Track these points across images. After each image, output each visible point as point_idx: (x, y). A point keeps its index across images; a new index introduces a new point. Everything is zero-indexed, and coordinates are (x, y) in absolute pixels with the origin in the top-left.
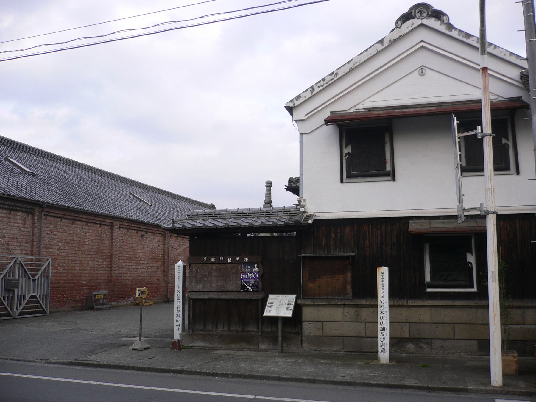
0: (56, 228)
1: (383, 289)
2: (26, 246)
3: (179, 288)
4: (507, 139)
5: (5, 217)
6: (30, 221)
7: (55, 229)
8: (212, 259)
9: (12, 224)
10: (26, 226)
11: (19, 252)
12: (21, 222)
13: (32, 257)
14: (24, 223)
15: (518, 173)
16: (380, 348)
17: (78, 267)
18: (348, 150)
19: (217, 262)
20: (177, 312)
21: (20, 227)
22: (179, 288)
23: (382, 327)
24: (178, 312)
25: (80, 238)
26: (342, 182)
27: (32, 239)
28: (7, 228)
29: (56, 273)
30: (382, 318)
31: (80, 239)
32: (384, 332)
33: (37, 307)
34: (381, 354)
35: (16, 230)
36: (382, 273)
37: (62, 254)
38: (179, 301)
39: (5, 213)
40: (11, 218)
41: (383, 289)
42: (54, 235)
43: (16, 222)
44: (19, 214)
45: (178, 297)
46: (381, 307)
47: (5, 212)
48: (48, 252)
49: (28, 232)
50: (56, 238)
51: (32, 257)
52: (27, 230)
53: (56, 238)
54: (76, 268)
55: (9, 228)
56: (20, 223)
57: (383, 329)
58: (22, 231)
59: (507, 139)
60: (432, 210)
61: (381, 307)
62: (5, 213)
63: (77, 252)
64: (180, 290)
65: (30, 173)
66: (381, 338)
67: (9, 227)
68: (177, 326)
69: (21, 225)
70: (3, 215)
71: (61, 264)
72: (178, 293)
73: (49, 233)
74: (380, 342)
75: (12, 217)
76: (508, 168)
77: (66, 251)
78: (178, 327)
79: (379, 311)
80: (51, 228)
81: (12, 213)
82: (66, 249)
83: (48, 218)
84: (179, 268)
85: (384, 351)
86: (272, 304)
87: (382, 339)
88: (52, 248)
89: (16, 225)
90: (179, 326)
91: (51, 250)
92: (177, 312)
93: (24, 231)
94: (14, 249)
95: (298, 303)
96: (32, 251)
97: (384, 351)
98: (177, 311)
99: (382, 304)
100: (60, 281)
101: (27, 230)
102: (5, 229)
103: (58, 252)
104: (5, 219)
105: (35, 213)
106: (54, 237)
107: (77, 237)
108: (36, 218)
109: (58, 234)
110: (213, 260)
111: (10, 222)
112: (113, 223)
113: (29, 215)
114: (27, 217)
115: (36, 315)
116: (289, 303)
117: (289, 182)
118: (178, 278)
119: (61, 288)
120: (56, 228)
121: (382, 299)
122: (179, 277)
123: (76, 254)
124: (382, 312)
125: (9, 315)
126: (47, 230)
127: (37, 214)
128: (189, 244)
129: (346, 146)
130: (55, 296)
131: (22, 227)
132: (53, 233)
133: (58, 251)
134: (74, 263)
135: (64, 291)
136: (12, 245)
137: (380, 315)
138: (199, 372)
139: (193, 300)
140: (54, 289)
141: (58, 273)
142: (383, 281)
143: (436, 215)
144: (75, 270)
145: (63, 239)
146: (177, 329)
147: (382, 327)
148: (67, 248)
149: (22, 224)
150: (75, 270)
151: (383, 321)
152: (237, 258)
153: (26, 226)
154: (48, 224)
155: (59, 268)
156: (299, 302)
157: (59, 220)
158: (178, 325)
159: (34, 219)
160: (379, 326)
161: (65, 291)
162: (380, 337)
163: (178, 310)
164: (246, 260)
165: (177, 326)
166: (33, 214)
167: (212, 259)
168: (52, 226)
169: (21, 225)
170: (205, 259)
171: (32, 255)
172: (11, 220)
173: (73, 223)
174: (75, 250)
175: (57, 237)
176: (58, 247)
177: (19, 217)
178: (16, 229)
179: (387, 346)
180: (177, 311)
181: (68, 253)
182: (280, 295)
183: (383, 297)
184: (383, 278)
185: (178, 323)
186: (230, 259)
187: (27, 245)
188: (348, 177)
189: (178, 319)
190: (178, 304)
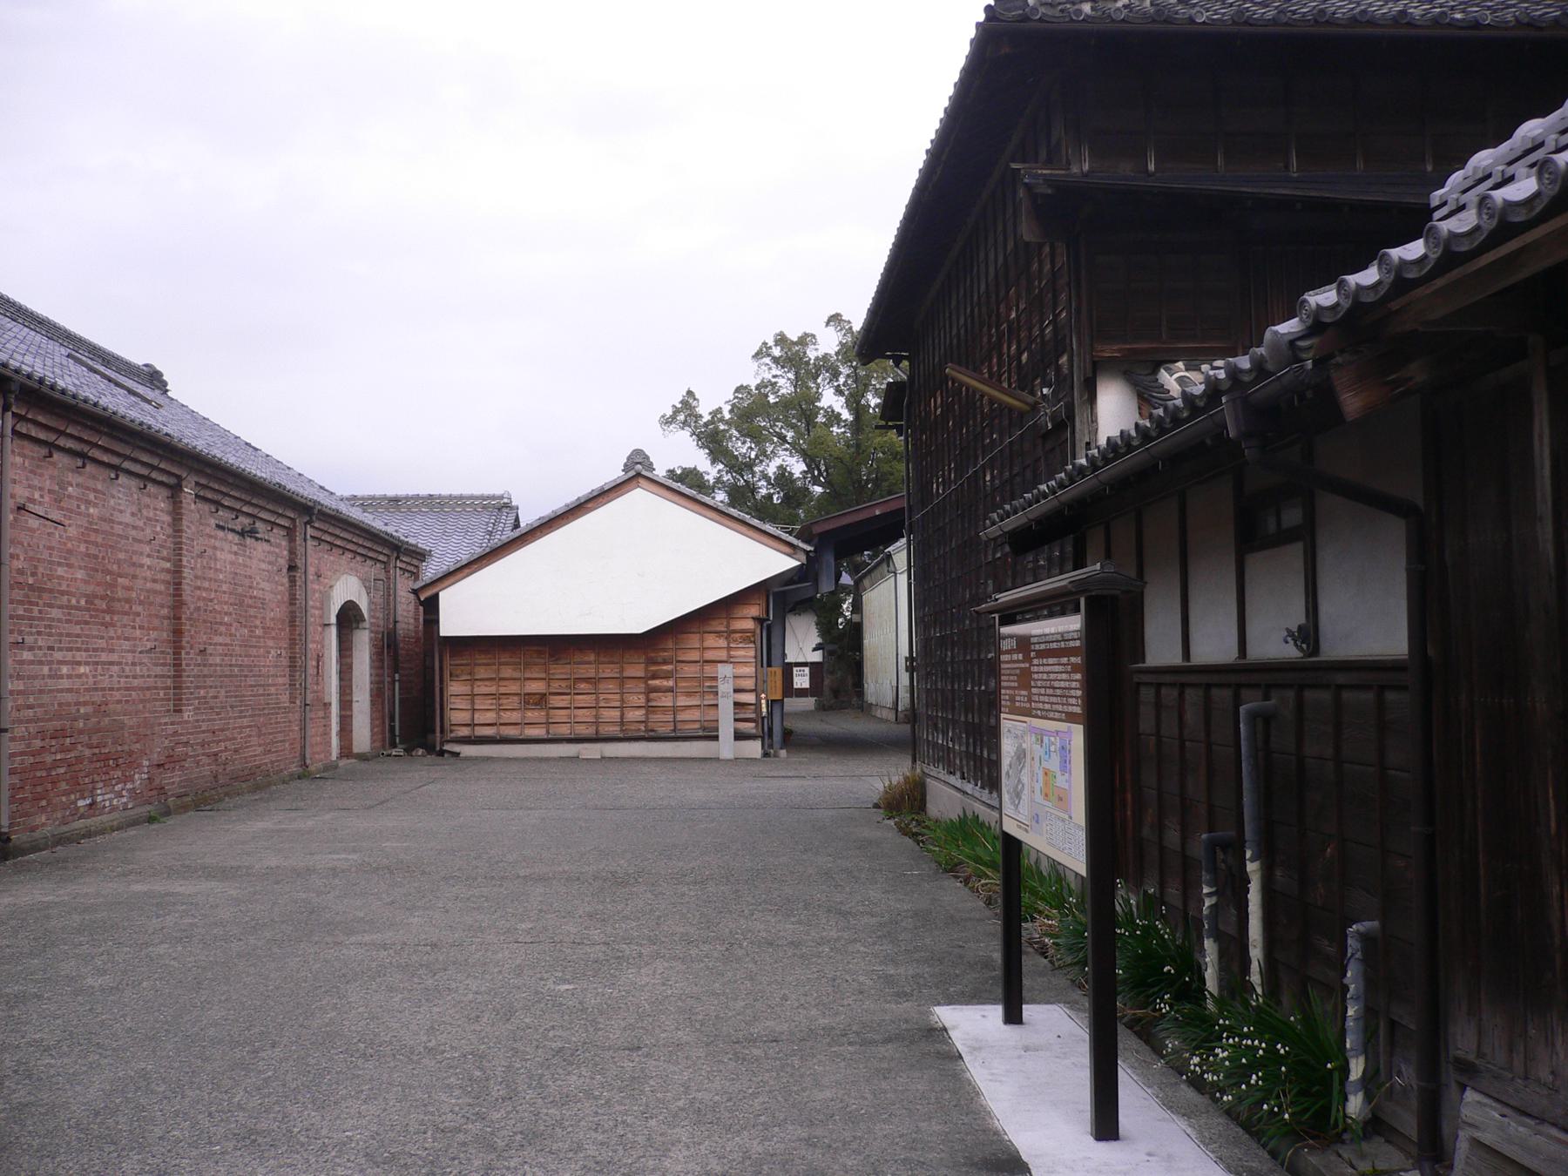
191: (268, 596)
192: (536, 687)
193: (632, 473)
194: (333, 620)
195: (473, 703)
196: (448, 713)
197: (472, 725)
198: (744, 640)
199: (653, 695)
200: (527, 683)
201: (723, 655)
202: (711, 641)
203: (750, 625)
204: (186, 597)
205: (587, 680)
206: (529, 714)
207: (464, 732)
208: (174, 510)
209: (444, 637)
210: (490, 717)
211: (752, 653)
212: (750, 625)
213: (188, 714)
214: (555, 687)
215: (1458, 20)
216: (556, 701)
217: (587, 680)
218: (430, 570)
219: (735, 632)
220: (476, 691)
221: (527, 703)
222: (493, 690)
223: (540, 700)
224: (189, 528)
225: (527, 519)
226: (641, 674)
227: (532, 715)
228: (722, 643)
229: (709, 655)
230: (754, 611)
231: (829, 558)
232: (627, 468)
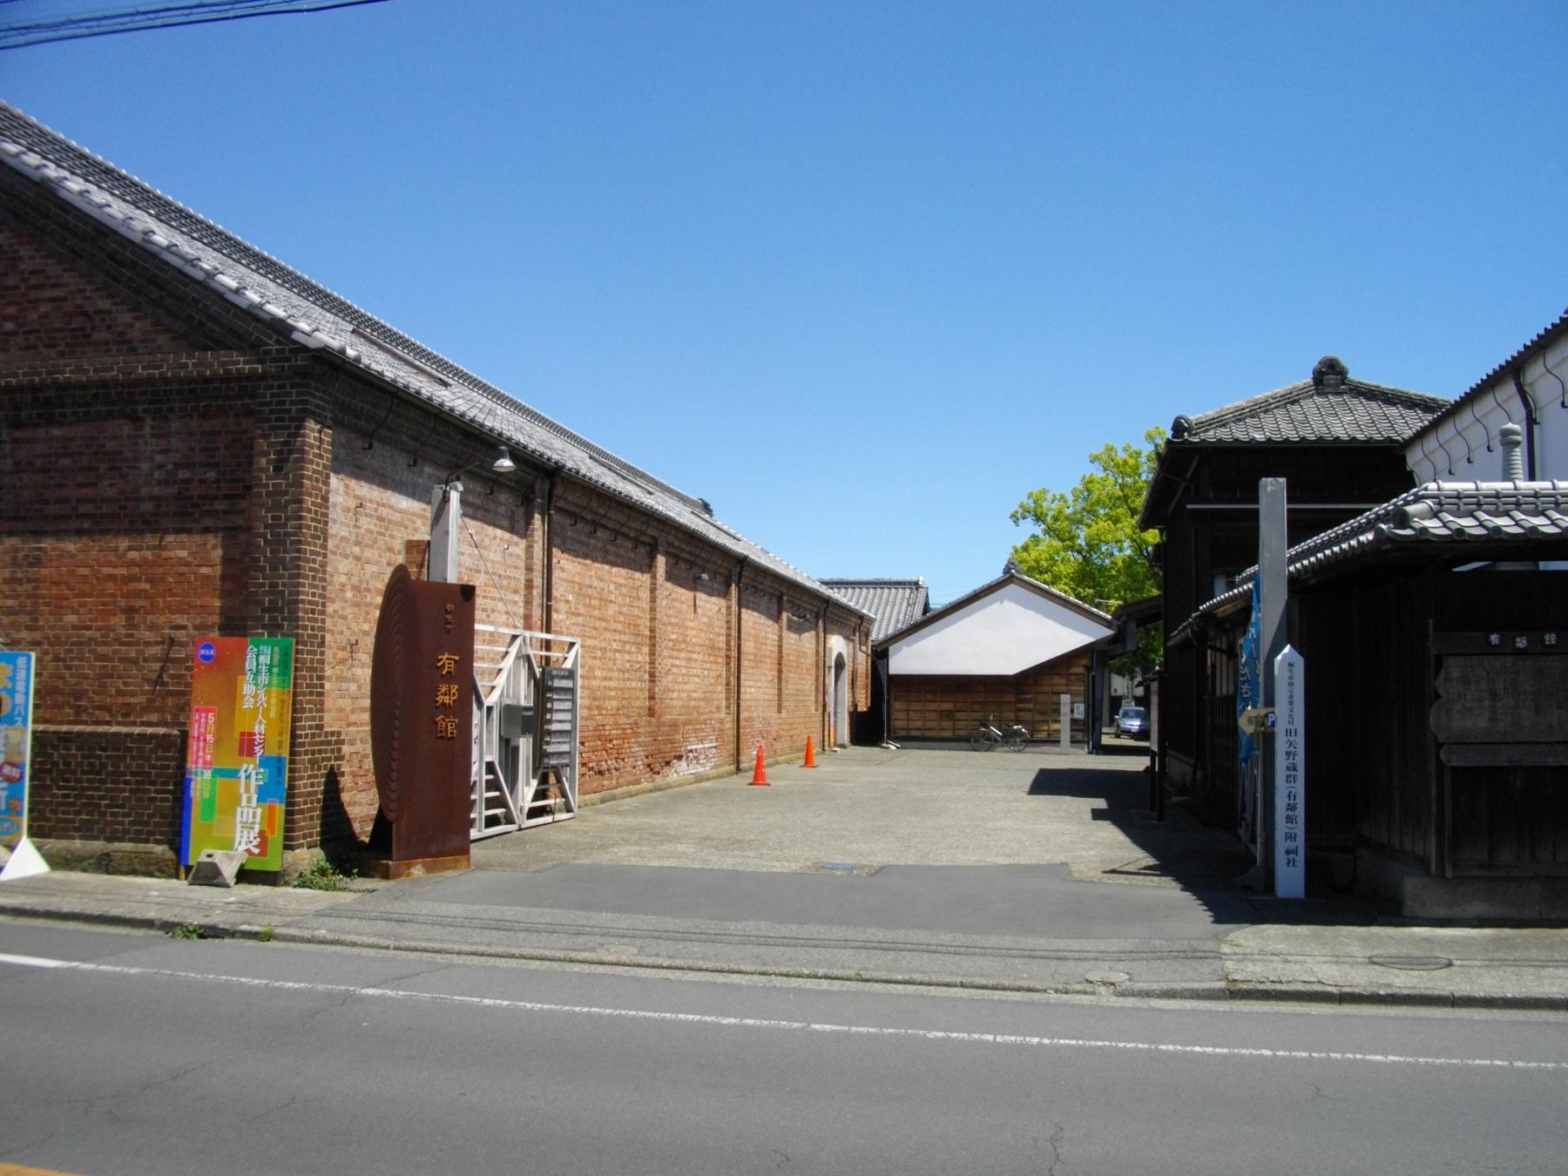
3: (1293, 734)
8: (1518, 640)
20: (1288, 809)
22: (1293, 734)
24: (1291, 807)
27: (526, 580)
31: (601, 585)
45: (1291, 761)
57: (1290, 837)
64: (1295, 739)
68: (1288, 852)
72: (1292, 749)
77: (580, 620)
78: (1291, 856)
84: (1291, 671)
90: (1296, 852)
92: (1288, 809)
98: (1289, 805)
110: (1521, 643)
112: (655, 539)
117: (1173, 429)
118: (1288, 700)
122: (1291, 697)
128: (377, 613)
139: (1456, 771)
146: (1288, 863)
148: (582, 610)
158: (1291, 848)
163: (1292, 801)
165: (1288, 852)
167: (1518, 640)
173: (591, 533)
180: (1289, 805)
185: (1291, 845)
189: (1293, 831)
190: (1292, 785)
191: (808, 651)
192: (948, 706)
193: (1008, 576)
194: (833, 664)
195: (908, 715)
196: (892, 722)
197: (908, 729)
198: (1077, 680)
199: (1019, 714)
200: (927, 704)
201: (1064, 688)
202: (1057, 680)
203: (1081, 670)
204: (784, 654)
205: (979, 703)
206: (942, 723)
207: (903, 733)
208: (213, 532)
209: (236, 679)
210: (918, 724)
211: (1082, 688)
212: (1081, 670)
213: (784, 714)
214: (959, 706)
215: (1046, 1045)
216: (959, 715)
217: (979, 703)
218: (878, 633)
219: (1072, 674)
220: (911, 708)
221: (941, 716)
222: (921, 708)
223: (949, 715)
224: (662, 602)
225: (938, 602)
226: (1013, 699)
227: (945, 724)
228: (1063, 681)
229: (1056, 689)
230: (1085, 662)
231: (1132, 626)
232: (1007, 570)
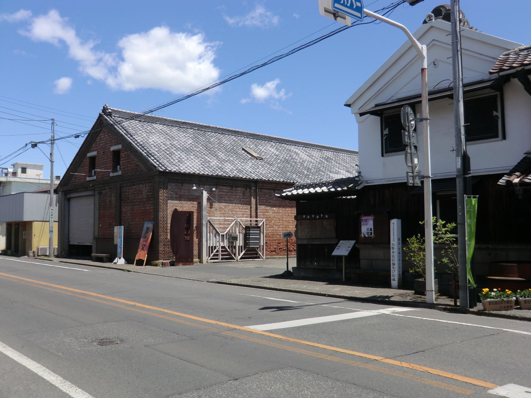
0: (270, 198)
1: (394, 235)
2: (246, 212)
4: (497, 111)
5: (228, 192)
6: (249, 194)
7: (270, 199)
9: (234, 197)
10: (246, 197)
11: (241, 215)
12: (241, 194)
13: (251, 219)
14: (244, 195)
15: (504, 138)
16: (392, 278)
17: (291, 225)
18: (386, 132)
19: (320, 218)
21: (240, 198)
23: (393, 262)
25: (292, 204)
26: (383, 156)
28: (230, 199)
29: (272, 230)
30: (393, 256)
32: (395, 266)
33: (254, 254)
34: (392, 282)
35: (237, 200)
36: (393, 224)
37: (277, 216)
38: (52, 229)
39: (228, 189)
40: (233, 192)
41: (394, 235)
42: (269, 202)
43: (237, 195)
44: (239, 189)
46: (392, 248)
47: (228, 188)
48: (264, 215)
49: (248, 201)
50: (271, 205)
51: (251, 219)
52: (246, 200)
53: (271, 205)
54: (290, 226)
55: (232, 199)
56: (240, 196)
58: (243, 201)
59: (497, 111)
60: (445, 174)
61: (392, 248)
62: (228, 189)
63: (290, 214)
65: (257, 158)
66: (393, 271)
67: (232, 199)
69: (241, 197)
70: (226, 191)
71: (276, 224)
73: (264, 201)
74: (392, 274)
75: (234, 191)
76: (497, 136)
77: (280, 214)
79: (392, 251)
80: (266, 197)
81: (234, 189)
82: (280, 213)
83: (263, 190)
85: (394, 280)
86: (339, 247)
87: (393, 271)
88: (267, 213)
89: (238, 197)
91: (267, 214)
93: (244, 201)
94: (237, 214)
95: (356, 246)
96: (251, 215)
97: (394, 280)
99: (393, 246)
100: (276, 236)
101: (246, 200)
102: (229, 200)
103: (273, 215)
104: (228, 194)
105: (251, 188)
106: (269, 204)
107: (289, 203)
108: (252, 191)
109: (272, 201)
111: (232, 195)
113: (247, 189)
114: (246, 191)
115: (254, 260)
116: (349, 246)
118: (393, 234)
119: (277, 241)
120: (270, 198)
121: (393, 243)
123: (289, 216)
124: (393, 252)
125: (234, 259)
126: (262, 200)
127: (253, 188)
129: (385, 129)
130: (272, 246)
131: (242, 198)
132: (268, 201)
133: (273, 214)
134: (288, 223)
135: (279, 243)
136: (235, 211)
137: (392, 254)
138: (240, 285)
140: (270, 241)
141: (274, 230)
142: (394, 229)
143: (439, 178)
144: (289, 228)
145: (277, 205)
147: (393, 262)
149: (242, 196)
150: (289, 228)
151: (394, 258)
152: (322, 215)
153: (246, 197)
154: (263, 195)
155: (274, 226)
156: (357, 246)
157: (273, 191)
159: (251, 192)
160: (392, 262)
161: (280, 243)
162: (392, 270)
164: (327, 216)
166: (250, 188)
168: (267, 196)
169: (241, 197)
170: (304, 216)
171: (251, 218)
172: (233, 194)
174: (288, 213)
175: (271, 204)
176: (273, 211)
177: (239, 191)
178: (238, 199)
179: (396, 276)
181: (281, 215)
182: (346, 241)
183: (394, 241)
184: (393, 227)
186: (318, 216)
187: (247, 211)
188: (386, 153)
